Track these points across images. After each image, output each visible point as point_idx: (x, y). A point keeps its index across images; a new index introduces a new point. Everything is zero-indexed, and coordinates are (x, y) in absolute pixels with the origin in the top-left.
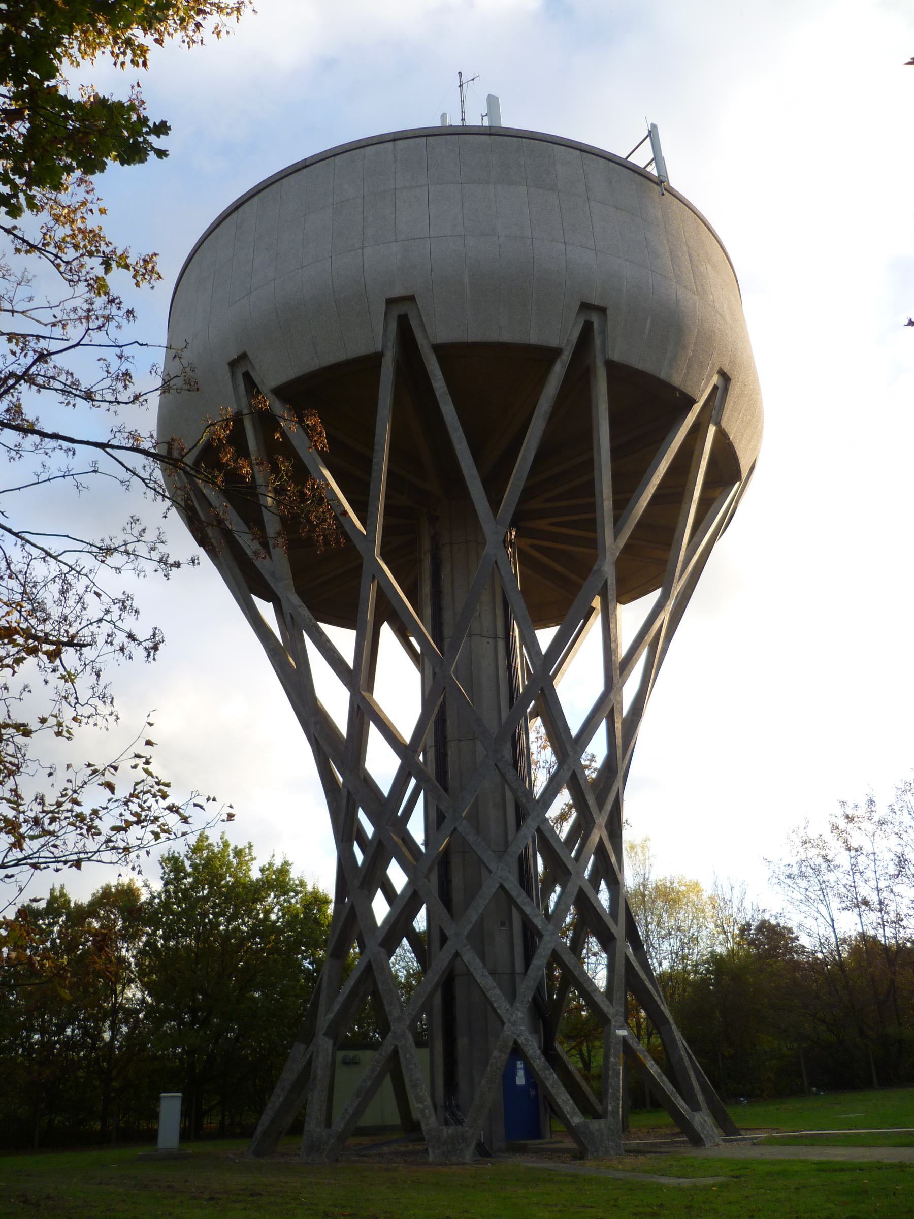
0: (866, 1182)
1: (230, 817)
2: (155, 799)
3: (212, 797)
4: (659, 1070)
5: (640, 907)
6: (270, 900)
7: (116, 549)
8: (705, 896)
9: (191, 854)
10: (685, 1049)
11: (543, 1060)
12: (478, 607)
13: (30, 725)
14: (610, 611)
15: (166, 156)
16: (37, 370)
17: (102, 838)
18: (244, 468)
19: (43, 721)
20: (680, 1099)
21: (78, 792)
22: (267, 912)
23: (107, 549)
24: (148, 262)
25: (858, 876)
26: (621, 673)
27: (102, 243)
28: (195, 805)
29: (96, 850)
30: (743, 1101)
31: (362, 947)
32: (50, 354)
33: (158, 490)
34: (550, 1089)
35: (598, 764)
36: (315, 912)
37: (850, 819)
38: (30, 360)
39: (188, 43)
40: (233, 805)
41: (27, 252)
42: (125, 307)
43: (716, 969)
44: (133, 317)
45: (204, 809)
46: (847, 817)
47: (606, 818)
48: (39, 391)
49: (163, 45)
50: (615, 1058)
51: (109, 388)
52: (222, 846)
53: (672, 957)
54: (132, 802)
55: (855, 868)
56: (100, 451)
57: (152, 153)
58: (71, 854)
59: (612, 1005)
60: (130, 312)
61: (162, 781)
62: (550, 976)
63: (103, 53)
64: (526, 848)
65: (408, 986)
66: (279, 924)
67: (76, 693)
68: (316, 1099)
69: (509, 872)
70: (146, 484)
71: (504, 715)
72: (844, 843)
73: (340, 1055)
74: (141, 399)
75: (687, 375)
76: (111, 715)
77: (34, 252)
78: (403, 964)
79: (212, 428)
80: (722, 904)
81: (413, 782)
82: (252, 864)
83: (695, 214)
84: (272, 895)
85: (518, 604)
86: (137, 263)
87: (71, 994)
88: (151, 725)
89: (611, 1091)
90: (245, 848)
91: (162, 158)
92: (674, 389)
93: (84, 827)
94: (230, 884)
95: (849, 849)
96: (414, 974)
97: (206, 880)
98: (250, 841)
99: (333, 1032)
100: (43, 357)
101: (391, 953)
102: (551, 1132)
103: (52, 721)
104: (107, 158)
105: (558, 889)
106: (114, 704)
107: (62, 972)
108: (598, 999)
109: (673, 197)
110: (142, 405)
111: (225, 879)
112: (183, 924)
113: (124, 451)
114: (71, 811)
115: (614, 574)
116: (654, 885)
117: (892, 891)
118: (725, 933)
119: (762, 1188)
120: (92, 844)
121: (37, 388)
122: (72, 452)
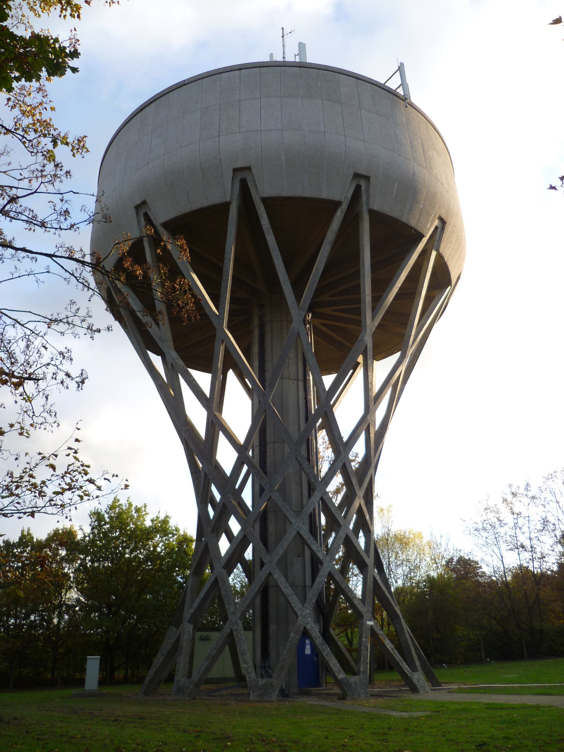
0: (515, 716)
1: (127, 486)
2: (81, 475)
3: (116, 475)
4: (393, 647)
5: (385, 547)
6: (157, 539)
7: (61, 321)
8: (425, 541)
9: (109, 510)
10: (409, 633)
11: (321, 639)
12: (287, 361)
13: (3, 428)
14: (369, 365)
15: (78, 71)
16: (10, 208)
17: (47, 499)
18: (138, 271)
19: (12, 426)
20: (405, 664)
21: (33, 470)
22: (155, 547)
23: (55, 320)
24: (80, 141)
25: (518, 530)
26: (374, 404)
27: (52, 129)
28: (105, 479)
29: (43, 506)
30: (445, 666)
31: (212, 569)
32: (18, 197)
33: (85, 283)
34: (325, 656)
35: (359, 459)
36: (185, 547)
37: (514, 495)
38: (5, 201)
39: (110, 3)
40: (128, 480)
41: (5, 134)
42: (65, 169)
43: (430, 585)
44: (70, 175)
45: (110, 482)
46: (513, 494)
47: (364, 492)
48: (11, 221)
49: (90, 4)
50: (365, 639)
51: (55, 220)
52: (128, 506)
53: (404, 578)
54: (66, 476)
55: (517, 525)
56: (49, 259)
57: (68, 70)
58: (28, 508)
59: (365, 606)
60: (68, 173)
61: (84, 465)
62: (328, 588)
63: (55, 9)
64: (314, 509)
65: (242, 594)
66: (162, 554)
67: (33, 409)
68: (182, 661)
69: (303, 524)
70: (77, 280)
71: (302, 428)
72: (510, 510)
73: (198, 634)
74: (75, 227)
75: (419, 219)
76: (54, 423)
77: (9, 134)
78: (239, 579)
79: (118, 246)
80: (435, 546)
81: (245, 468)
82: (146, 517)
83: (426, 119)
84: (158, 536)
85: (312, 361)
86: (73, 142)
87: (24, 593)
88: (78, 429)
89: (362, 658)
90: (142, 507)
91: (75, 73)
92: (411, 228)
93: (36, 491)
94: (133, 529)
95: (513, 514)
96: (246, 585)
97: (118, 526)
98: (145, 503)
99: (193, 620)
100: (13, 200)
101: (230, 573)
102: (326, 684)
103: (17, 426)
104: (40, 73)
105: (333, 535)
106: (57, 416)
107: (18, 580)
108: (356, 602)
109: (413, 108)
110: (76, 231)
111: (129, 525)
112: (103, 553)
113: (63, 259)
114: (29, 481)
115: (371, 342)
116: (393, 534)
117: (539, 540)
118: (436, 563)
119: (452, 719)
120: (40, 502)
121: (10, 219)
122: (35, 260)
